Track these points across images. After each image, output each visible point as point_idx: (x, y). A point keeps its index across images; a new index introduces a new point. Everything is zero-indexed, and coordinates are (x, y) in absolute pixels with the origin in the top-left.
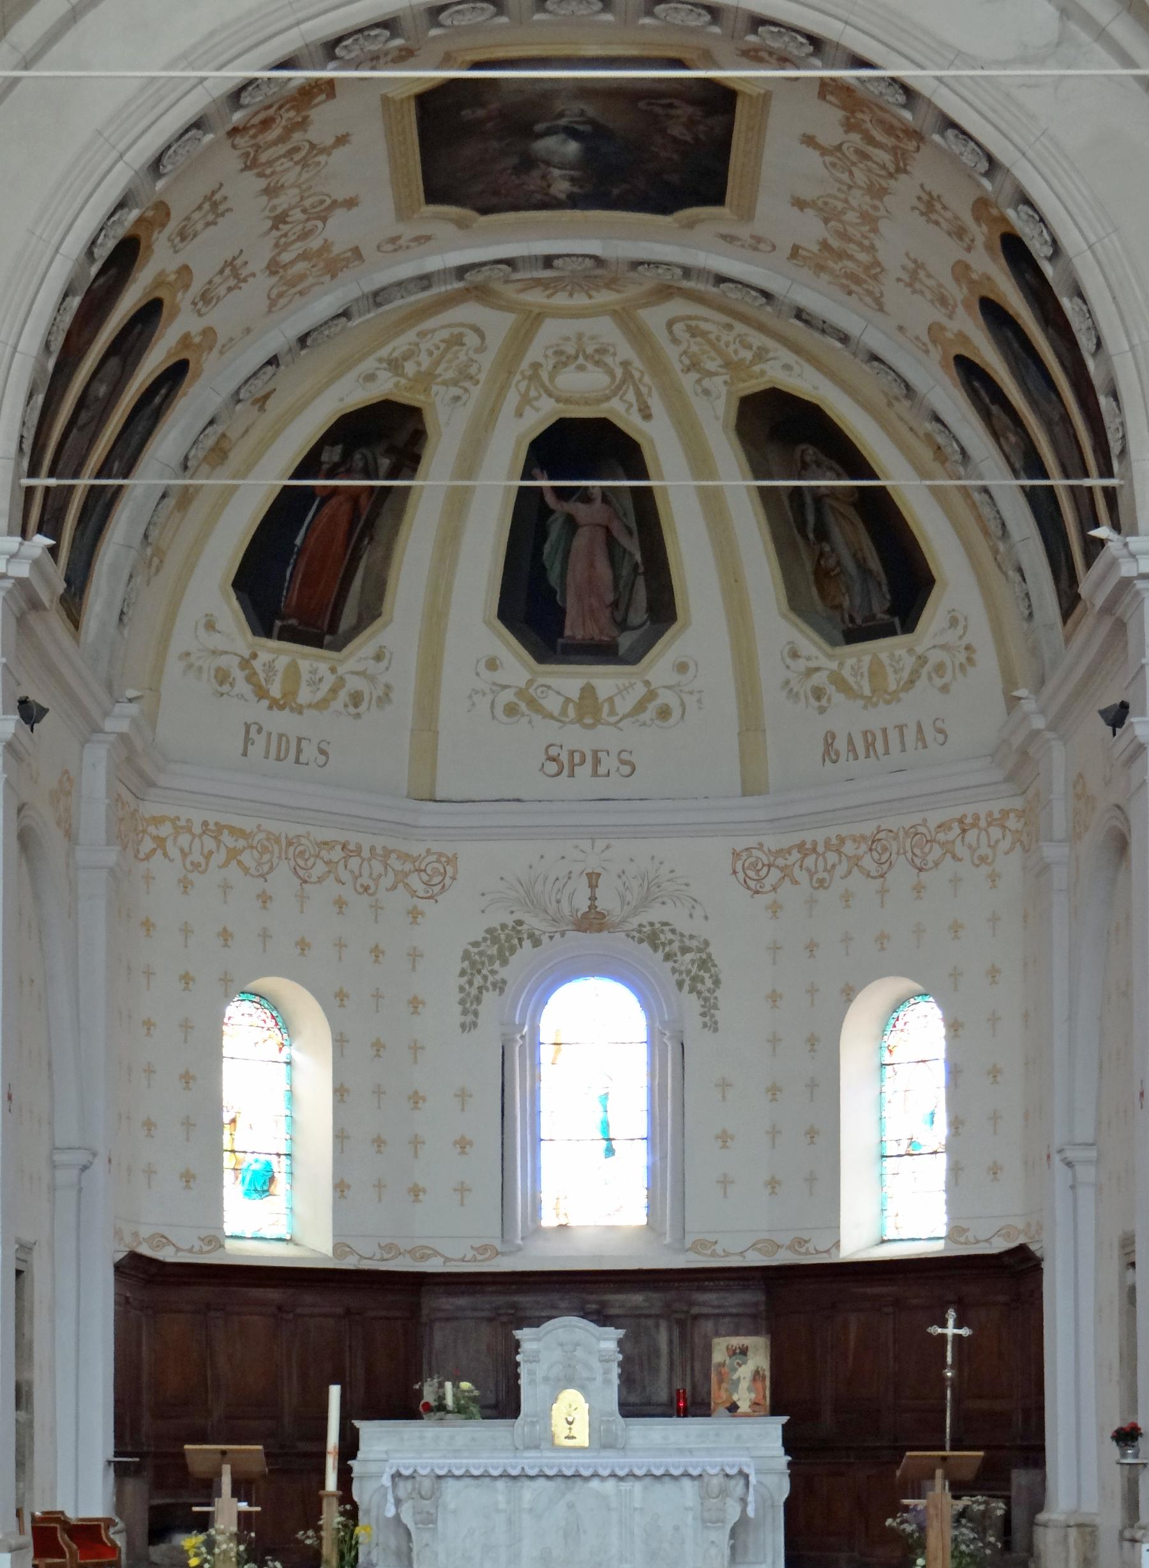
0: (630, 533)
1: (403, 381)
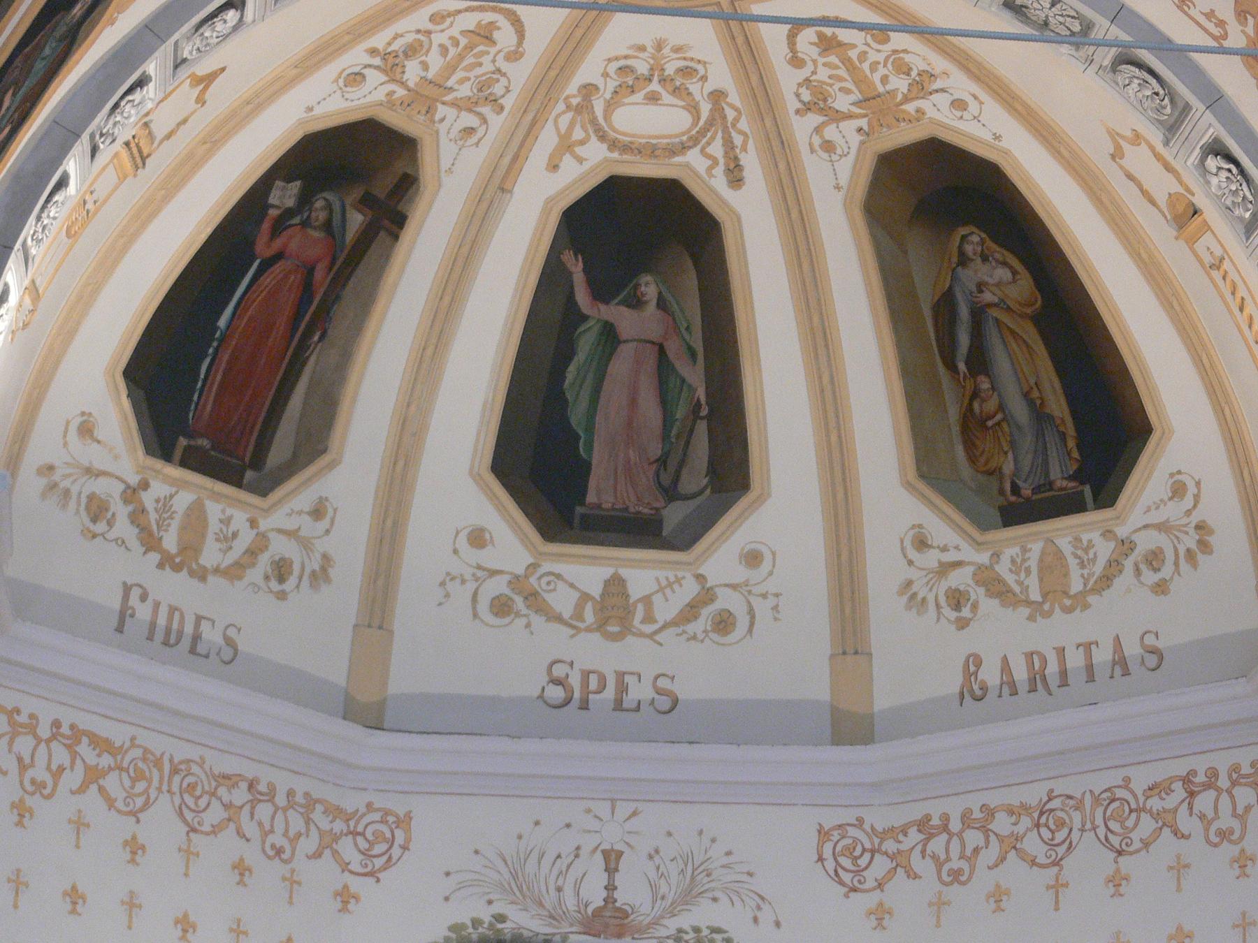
0: (693, 355)
1: (401, 92)
